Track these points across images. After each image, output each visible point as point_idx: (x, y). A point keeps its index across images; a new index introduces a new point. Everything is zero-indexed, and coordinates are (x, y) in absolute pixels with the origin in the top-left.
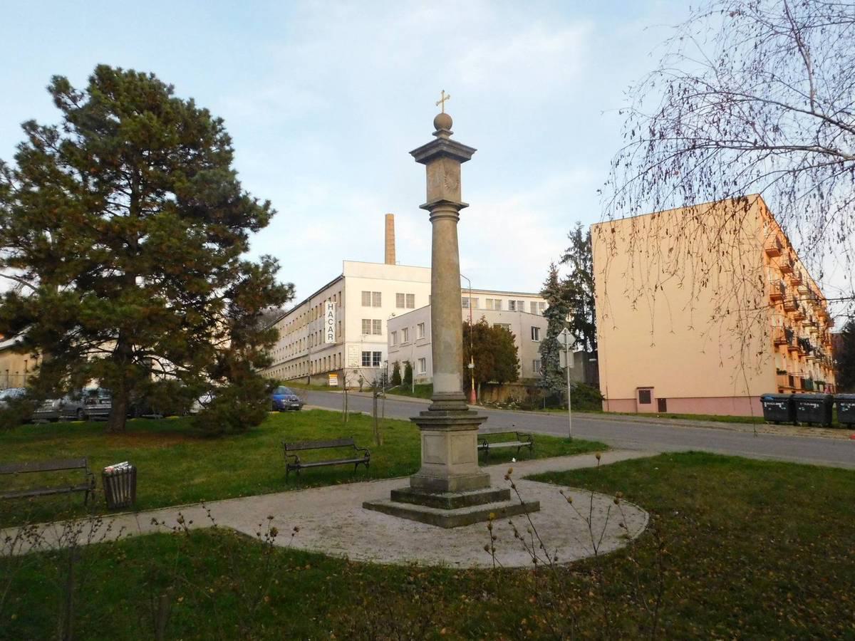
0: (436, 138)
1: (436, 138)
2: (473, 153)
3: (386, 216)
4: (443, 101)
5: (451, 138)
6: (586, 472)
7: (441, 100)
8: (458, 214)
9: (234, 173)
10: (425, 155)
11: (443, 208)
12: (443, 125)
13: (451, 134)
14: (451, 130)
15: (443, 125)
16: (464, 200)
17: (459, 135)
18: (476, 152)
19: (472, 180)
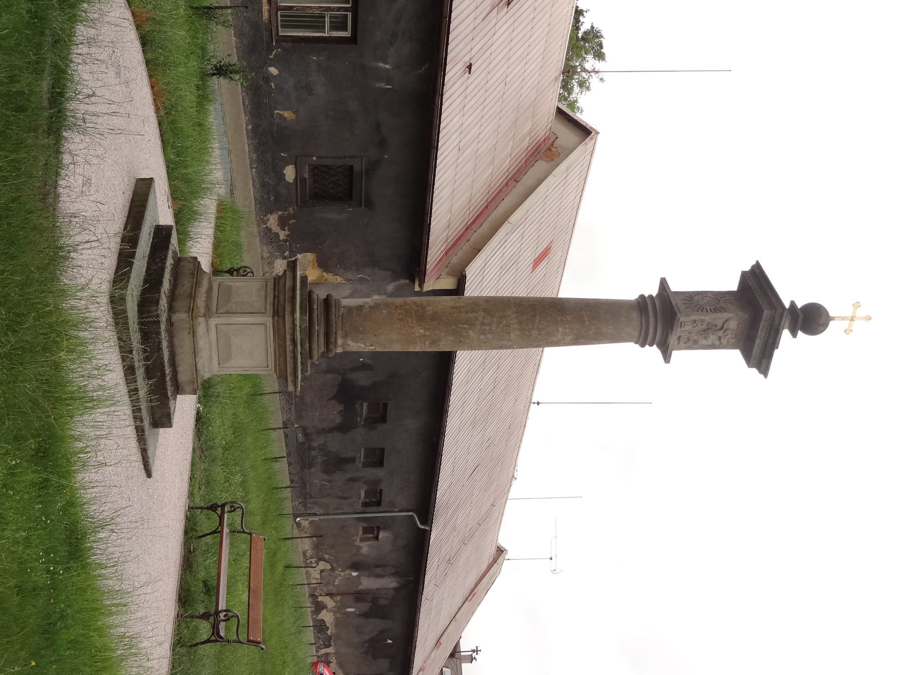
0: (787, 305)
1: (787, 305)
2: (760, 372)
3: (151, 179)
4: (852, 319)
5: (786, 334)
6: (48, 631)
7: (849, 315)
8: (651, 345)
9: (793, 304)
10: (756, 282)
11: (663, 319)
12: (811, 319)
13: (794, 335)
14: (800, 333)
15: (811, 319)
16: (676, 354)
17: (791, 346)
18: (762, 376)
19: (720, 366)
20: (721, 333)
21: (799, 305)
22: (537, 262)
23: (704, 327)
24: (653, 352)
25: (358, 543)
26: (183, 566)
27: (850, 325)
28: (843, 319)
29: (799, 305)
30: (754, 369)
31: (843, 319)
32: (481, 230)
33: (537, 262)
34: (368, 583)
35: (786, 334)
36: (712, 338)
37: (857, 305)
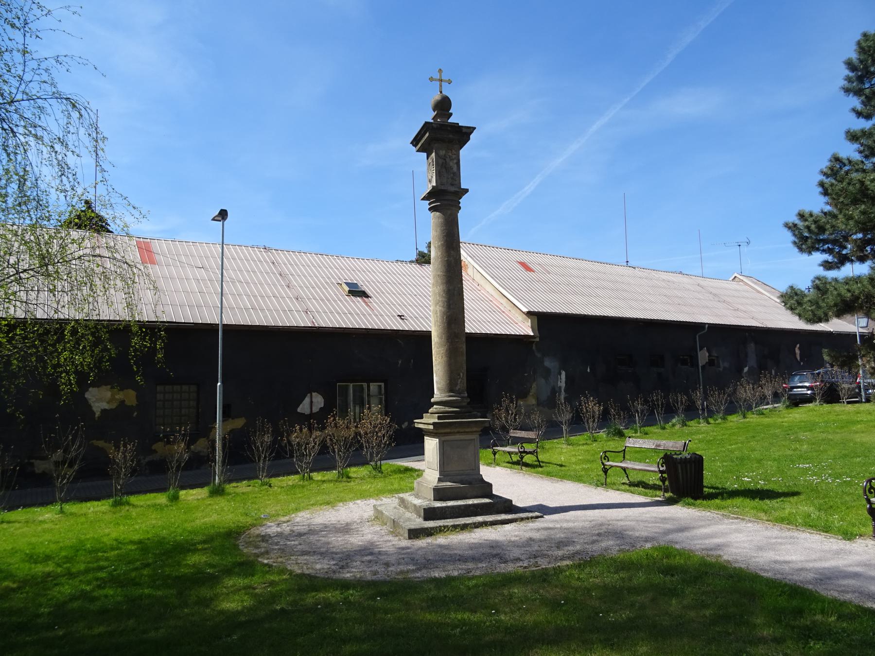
7: (438, 83)
12: (443, 106)
15: (443, 106)
20: (448, 160)
21: (854, 56)
22: (523, 265)
23: (444, 170)
24: (463, 201)
25: (721, 369)
26: (161, 542)
27: (446, 81)
28: (441, 86)
29: (854, 56)
30: (471, 136)
31: (441, 86)
32: (505, 304)
33: (523, 265)
34: (752, 361)
35: (451, 120)
36: (452, 164)
37: (431, 79)
